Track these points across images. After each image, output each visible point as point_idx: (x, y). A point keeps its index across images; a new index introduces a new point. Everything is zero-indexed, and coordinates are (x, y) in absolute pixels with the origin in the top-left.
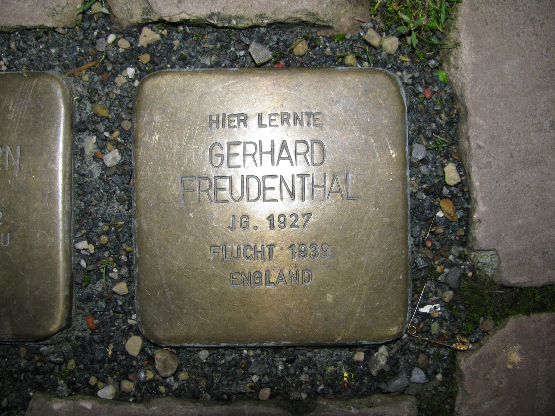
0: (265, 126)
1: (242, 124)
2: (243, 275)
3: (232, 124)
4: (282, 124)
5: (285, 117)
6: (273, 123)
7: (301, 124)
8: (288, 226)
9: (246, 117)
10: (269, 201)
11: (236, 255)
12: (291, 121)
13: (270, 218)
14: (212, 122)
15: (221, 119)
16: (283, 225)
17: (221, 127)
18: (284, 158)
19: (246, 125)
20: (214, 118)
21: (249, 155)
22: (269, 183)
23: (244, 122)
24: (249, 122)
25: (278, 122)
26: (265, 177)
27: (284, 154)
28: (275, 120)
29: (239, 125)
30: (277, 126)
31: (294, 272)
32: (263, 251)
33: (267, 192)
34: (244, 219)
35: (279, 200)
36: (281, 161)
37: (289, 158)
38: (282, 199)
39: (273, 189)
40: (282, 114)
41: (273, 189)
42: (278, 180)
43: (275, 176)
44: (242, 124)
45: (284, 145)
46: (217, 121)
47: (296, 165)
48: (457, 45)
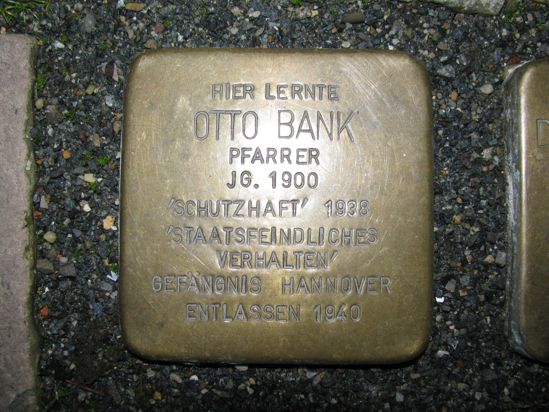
0: (273, 98)
2: (291, 307)
5: (297, 89)
6: (282, 96)
9: (253, 89)
12: (303, 94)
19: (252, 97)
23: (316, 157)
24: (256, 93)
25: (288, 92)
27: (305, 127)
28: (283, 92)
30: (285, 98)
35: (290, 98)
36: (301, 134)
37: (310, 131)
46: (220, 92)
47: (318, 139)
48: (425, 278)
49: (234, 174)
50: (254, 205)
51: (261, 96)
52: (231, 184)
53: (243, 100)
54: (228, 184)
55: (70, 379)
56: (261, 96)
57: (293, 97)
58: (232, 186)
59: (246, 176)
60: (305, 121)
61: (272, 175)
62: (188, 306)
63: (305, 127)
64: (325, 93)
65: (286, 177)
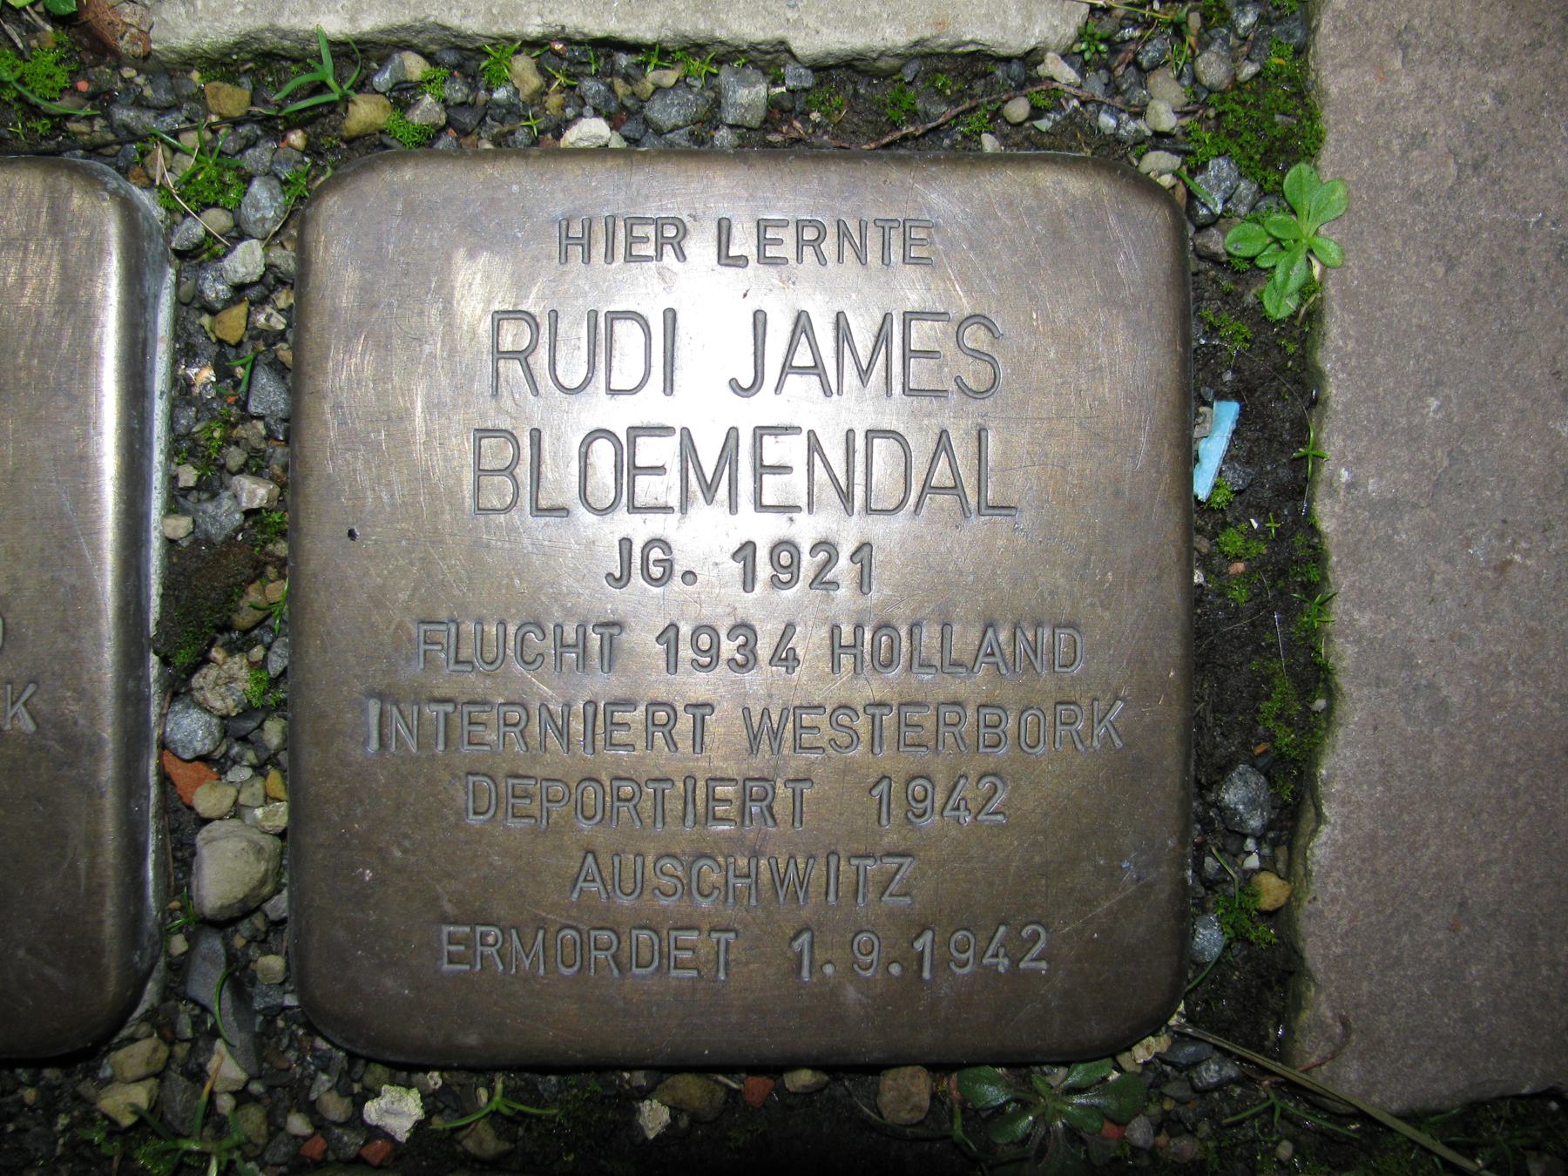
3: (639, 250)
4: (799, 259)
5: (810, 234)
6: (771, 251)
7: (861, 259)
8: (677, 579)
9: (683, 231)
12: (829, 246)
13: (745, 552)
14: (566, 240)
16: (785, 577)
18: (802, 370)
19: (681, 256)
20: (576, 231)
24: (690, 247)
26: (635, 432)
27: (803, 357)
28: (778, 242)
29: (659, 255)
31: (775, 718)
33: (642, 481)
34: (657, 553)
35: (792, 262)
36: (792, 379)
37: (817, 368)
39: (659, 470)
40: (800, 225)
41: (659, 470)
43: (664, 431)
45: (802, 325)
51: (701, 248)
52: (618, 575)
53: (653, 265)
54: (610, 575)
55: (232, 649)
56: (701, 248)
58: (620, 580)
59: (657, 553)
62: (471, 778)
63: (803, 357)
65: (785, 558)
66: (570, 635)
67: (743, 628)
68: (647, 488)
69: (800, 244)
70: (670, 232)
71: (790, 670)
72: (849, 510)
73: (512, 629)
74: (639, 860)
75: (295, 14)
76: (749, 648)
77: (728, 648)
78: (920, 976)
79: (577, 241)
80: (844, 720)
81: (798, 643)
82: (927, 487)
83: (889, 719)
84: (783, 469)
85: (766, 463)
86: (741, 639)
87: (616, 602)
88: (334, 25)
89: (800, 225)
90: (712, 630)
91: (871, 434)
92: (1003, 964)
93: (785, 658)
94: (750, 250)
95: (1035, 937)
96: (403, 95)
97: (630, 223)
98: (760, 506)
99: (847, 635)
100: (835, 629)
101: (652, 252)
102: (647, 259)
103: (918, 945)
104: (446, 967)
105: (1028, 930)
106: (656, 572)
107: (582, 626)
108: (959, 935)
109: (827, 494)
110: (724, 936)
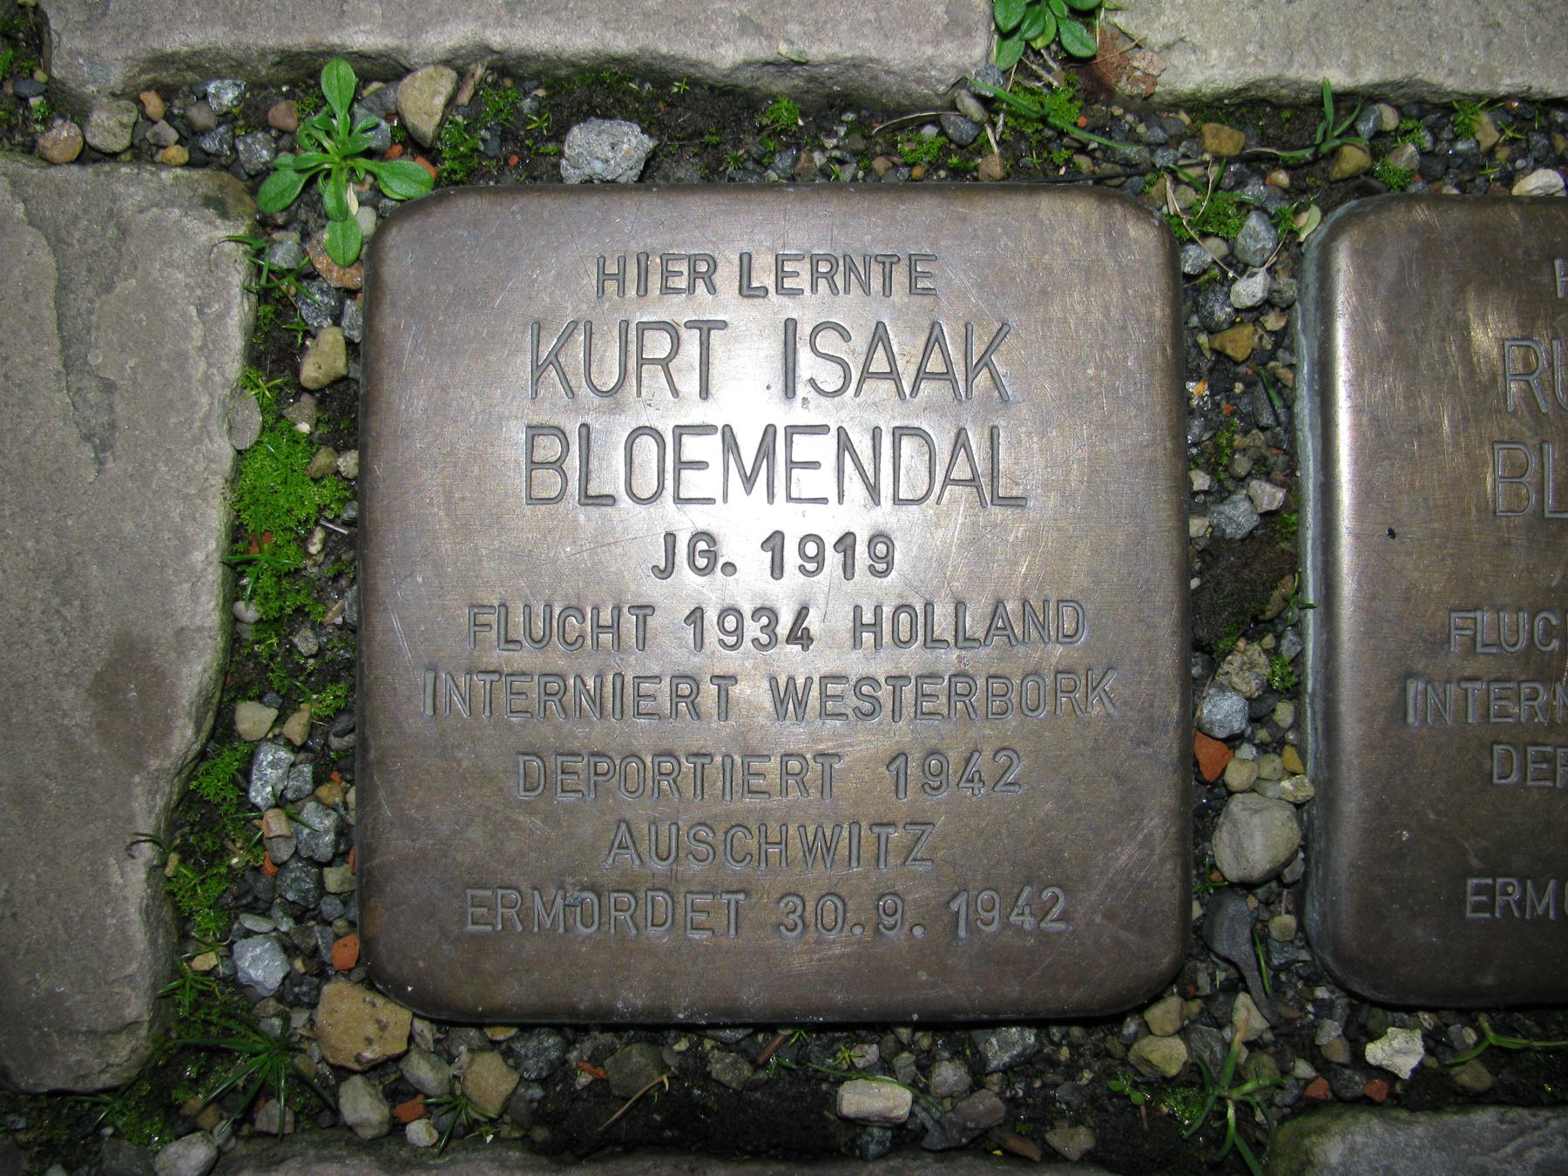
1: (701, 287)
4: (814, 288)
6: (788, 283)
9: (713, 265)
10: (800, 500)
11: (538, 631)
14: (603, 276)
15: (632, 271)
17: (632, 292)
18: (879, 376)
19: (712, 289)
21: (653, 361)
22: (694, 448)
24: (718, 279)
27: (880, 364)
28: (926, 275)
29: (691, 289)
31: (590, 683)
32: (615, 627)
33: (686, 474)
34: (702, 546)
35: (807, 292)
38: (725, 499)
39: (815, 465)
41: (815, 465)
42: (830, 441)
43: (822, 429)
44: (701, 287)
46: (621, 278)
49: (670, 538)
50: (611, 286)
52: (662, 566)
57: (814, 288)
60: (880, 351)
61: (770, 544)
64: (900, 276)
65: (811, 549)
66: (606, 617)
67: (767, 612)
68: (695, 484)
69: (815, 276)
70: (703, 267)
71: (805, 648)
72: (877, 502)
73: (557, 611)
74: (837, 830)
75: (1303, 66)
76: (770, 629)
77: (752, 629)
78: (956, 936)
79: (702, 276)
80: (866, 689)
81: (813, 622)
82: (948, 480)
83: (908, 692)
84: (700, 465)
85: (684, 459)
86: (765, 620)
87: (654, 590)
88: (1337, 78)
89: (815, 261)
90: (737, 612)
91: (899, 433)
92: (1029, 922)
93: (800, 636)
94: (770, 282)
95: (1056, 899)
96: (1381, 143)
97: (666, 259)
98: (678, 499)
99: (868, 617)
100: (857, 609)
101: (684, 285)
102: (678, 291)
103: (954, 906)
104: (470, 928)
105: (1047, 894)
106: (702, 562)
107: (617, 609)
108: (985, 895)
109: (855, 487)
110: (733, 897)
